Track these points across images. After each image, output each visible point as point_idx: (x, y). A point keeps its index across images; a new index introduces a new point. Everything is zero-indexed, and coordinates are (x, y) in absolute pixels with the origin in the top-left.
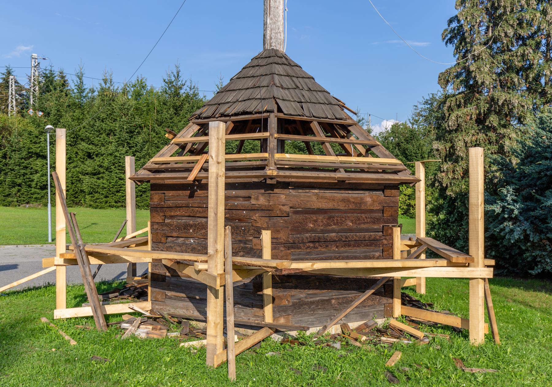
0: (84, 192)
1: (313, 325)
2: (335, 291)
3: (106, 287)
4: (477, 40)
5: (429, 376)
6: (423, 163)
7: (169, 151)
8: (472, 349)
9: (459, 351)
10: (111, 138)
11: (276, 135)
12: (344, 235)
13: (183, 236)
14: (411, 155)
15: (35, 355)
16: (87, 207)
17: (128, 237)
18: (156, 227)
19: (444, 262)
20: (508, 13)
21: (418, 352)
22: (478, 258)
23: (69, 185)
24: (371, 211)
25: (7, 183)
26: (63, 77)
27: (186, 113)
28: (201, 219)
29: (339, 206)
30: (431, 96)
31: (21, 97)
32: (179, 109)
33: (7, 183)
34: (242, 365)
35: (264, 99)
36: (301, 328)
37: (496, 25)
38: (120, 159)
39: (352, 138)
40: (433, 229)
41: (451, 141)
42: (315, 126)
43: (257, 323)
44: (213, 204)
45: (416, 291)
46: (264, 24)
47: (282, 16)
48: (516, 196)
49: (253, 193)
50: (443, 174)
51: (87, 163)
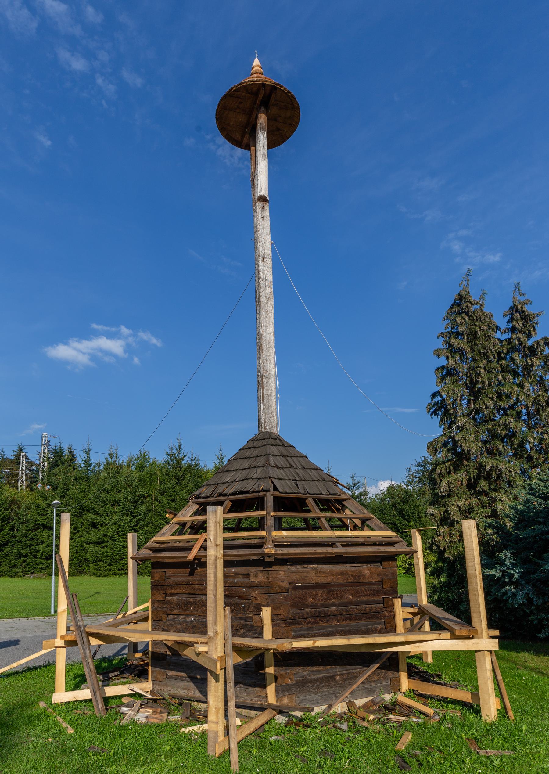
0: (89, 561)
1: (318, 704)
2: (339, 667)
3: (106, 664)
4: (460, 412)
5: (442, 762)
6: (419, 531)
7: (169, 530)
8: (485, 727)
9: (472, 730)
10: (115, 508)
11: (272, 514)
12: (345, 609)
13: (183, 614)
14: (408, 515)
15: (31, 746)
16: (90, 575)
17: (129, 613)
18: (156, 605)
19: (448, 635)
20: (486, 388)
21: (428, 731)
22: (482, 630)
23: (74, 555)
24: (371, 583)
25: (13, 555)
26: (71, 452)
27: (188, 483)
28: (201, 597)
29: (338, 579)
30: (423, 459)
31: (30, 472)
32: (181, 479)
33: (13, 555)
34: (245, 753)
35: (259, 479)
36: (305, 710)
37: (476, 398)
38: (123, 528)
39: (347, 512)
40: (435, 592)
41: (444, 505)
42: (310, 502)
43: (260, 705)
44: (212, 585)
45: (422, 660)
46: (258, 410)
47: (274, 402)
48: (514, 560)
49: (252, 570)
50: (440, 538)
51: (91, 532)
